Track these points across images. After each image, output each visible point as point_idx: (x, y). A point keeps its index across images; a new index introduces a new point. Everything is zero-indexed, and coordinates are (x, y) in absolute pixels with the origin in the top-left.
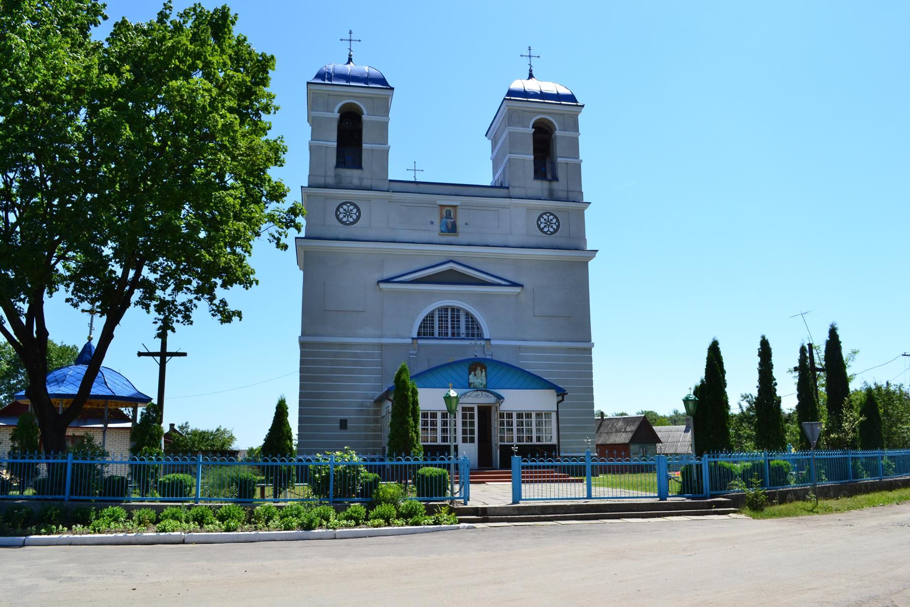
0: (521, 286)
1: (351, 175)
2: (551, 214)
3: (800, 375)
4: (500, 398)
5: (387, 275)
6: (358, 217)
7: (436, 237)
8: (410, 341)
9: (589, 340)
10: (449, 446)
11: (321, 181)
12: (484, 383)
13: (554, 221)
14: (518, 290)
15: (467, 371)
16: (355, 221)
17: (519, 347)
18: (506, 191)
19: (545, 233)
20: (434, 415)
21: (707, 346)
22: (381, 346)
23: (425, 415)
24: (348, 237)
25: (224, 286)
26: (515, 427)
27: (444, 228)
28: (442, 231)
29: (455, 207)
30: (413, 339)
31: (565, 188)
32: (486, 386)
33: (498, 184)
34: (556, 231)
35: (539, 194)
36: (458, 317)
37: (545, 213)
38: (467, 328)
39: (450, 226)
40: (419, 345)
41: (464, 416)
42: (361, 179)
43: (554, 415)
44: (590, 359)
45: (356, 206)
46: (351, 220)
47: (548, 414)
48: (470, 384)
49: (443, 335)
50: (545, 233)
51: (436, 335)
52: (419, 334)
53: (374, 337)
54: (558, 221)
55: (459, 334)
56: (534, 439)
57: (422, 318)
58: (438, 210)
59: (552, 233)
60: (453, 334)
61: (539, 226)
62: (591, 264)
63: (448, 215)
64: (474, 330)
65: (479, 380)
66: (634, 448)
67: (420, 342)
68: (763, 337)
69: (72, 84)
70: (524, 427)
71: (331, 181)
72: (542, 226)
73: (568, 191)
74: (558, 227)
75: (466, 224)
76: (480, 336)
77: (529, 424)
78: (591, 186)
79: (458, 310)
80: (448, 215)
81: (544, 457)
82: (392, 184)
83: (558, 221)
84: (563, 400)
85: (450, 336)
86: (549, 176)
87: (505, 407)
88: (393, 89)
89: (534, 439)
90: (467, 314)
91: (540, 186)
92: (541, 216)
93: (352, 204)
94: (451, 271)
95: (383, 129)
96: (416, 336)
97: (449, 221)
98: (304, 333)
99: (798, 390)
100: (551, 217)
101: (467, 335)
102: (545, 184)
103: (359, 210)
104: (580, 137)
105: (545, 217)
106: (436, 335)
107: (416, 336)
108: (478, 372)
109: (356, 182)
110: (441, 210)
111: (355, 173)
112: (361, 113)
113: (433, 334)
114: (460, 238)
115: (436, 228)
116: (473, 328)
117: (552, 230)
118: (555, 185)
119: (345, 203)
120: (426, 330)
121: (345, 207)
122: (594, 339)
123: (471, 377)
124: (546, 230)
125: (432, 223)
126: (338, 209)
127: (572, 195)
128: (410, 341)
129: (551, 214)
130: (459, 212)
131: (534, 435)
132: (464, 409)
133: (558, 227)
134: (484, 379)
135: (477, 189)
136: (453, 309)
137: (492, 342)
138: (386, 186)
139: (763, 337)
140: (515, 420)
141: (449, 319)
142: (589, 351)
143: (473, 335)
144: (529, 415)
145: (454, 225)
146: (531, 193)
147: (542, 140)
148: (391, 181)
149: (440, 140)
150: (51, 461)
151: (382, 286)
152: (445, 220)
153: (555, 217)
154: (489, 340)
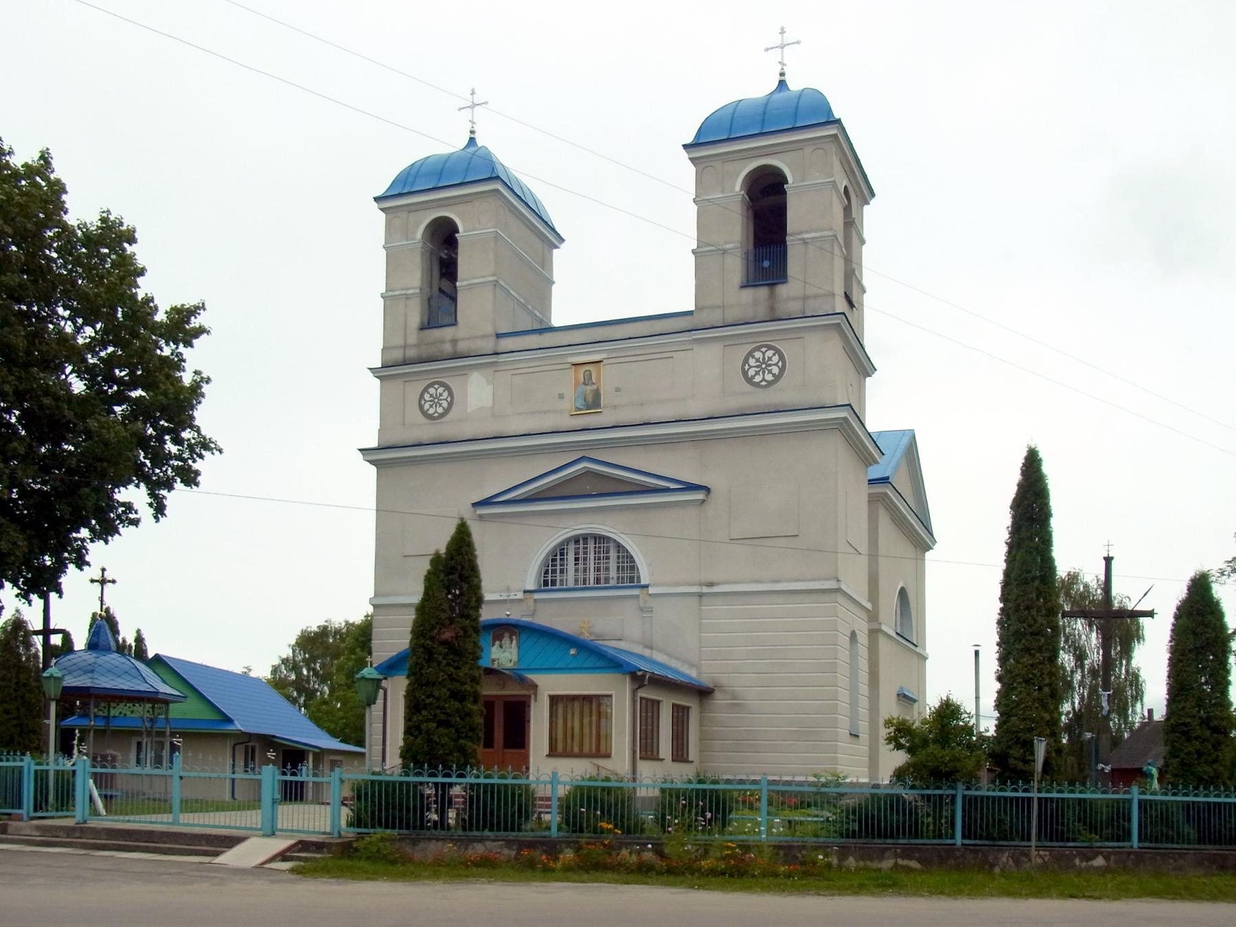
0: (707, 490)
8: (520, 596)
10: (1030, 799)
14: (700, 496)
19: (757, 385)
21: (1191, 574)
25: (97, 535)
27: (580, 403)
30: (525, 592)
31: (402, 343)
35: (749, 314)
39: (590, 399)
40: (535, 601)
50: (757, 385)
51: (571, 584)
54: (782, 358)
55: (607, 580)
60: (598, 581)
61: (745, 373)
63: (588, 380)
65: (507, 654)
72: (751, 372)
74: (782, 370)
75: (617, 390)
80: (588, 380)
83: (782, 358)
85: (613, 583)
94: (589, 473)
96: (531, 587)
97: (589, 388)
108: (506, 641)
109: (448, 348)
111: (448, 333)
112: (784, 180)
115: (568, 404)
117: (769, 377)
118: (782, 290)
125: (561, 396)
128: (520, 596)
133: (782, 370)
135: (638, 324)
137: (651, 590)
145: (597, 394)
146: (731, 315)
150: (99, 770)
152: (582, 388)
154: (646, 586)
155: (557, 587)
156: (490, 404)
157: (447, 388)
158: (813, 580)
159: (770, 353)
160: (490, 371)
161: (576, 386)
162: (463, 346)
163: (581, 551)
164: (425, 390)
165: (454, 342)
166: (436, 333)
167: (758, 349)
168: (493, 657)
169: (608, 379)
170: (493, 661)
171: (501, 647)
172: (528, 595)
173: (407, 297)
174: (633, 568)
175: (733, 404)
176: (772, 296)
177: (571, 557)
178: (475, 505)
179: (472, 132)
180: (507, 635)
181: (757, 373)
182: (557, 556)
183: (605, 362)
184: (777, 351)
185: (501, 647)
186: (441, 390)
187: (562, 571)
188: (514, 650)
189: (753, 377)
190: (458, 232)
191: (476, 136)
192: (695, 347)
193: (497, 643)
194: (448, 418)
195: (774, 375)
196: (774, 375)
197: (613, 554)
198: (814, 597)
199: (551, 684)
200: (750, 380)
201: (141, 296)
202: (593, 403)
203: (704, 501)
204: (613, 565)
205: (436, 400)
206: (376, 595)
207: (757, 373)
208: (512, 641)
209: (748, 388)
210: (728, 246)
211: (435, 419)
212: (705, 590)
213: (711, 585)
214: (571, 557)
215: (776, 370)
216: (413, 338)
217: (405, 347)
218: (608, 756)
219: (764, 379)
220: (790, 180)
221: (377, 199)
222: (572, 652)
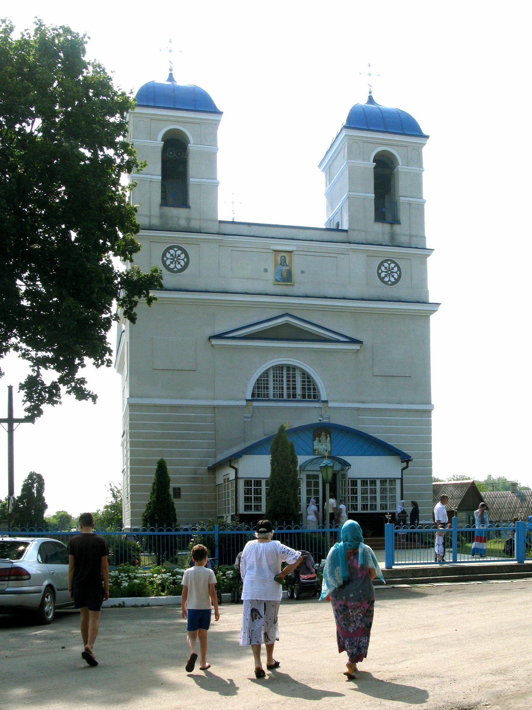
1: (178, 214)
2: (393, 262)
4: (346, 464)
5: (219, 330)
6: (187, 264)
7: (271, 288)
8: (244, 403)
9: (429, 402)
12: (329, 449)
13: (396, 269)
14: (357, 347)
15: (311, 436)
17: (358, 409)
18: (345, 234)
19: (386, 283)
20: (258, 483)
22: (214, 407)
23: (248, 483)
24: (178, 286)
26: (359, 495)
27: (278, 277)
28: (277, 281)
29: (291, 252)
30: (247, 400)
32: (330, 452)
33: (334, 226)
35: (380, 239)
36: (294, 377)
37: (386, 261)
38: (303, 389)
39: (285, 274)
40: (254, 408)
41: (308, 484)
42: (188, 219)
43: (398, 482)
44: (429, 423)
45: (184, 251)
46: (179, 267)
47: (392, 481)
48: (314, 451)
49: (280, 397)
50: (386, 283)
51: (271, 397)
52: (253, 395)
53: (206, 399)
54: (399, 269)
55: (294, 396)
56: (378, 507)
57: (257, 377)
58: (272, 256)
59: (393, 283)
60: (289, 396)
61: (379, 275)
62: (432, 317)
63: (283, 262)
64: (310, 392)
65: (324, 446)
67: (255, 404)
68: (95, 403)
69: (50, 177)
70: (253, 496)
71: (156, 221)
72: (383, 275)
73: (411, 236)
75: (303, 272)
76: (316, 397)
77: (374, 491)
78: (434, 232)
79: (294, 368)
80: (283, 262)
81: (400, 525)
82: (223, 225)
83: (399, 269)
84: (407, 467)
85: (299, 398)
86: (389, 217)
87: (352, 473)
88: (221, 113)
89: (378, 507)
90: (304, 374)
91: (381, 230)
92: (382, 264)
93: (180, 248)
94: (287, 325)
95: (211, 159)
96: (249, 397)
97: (285, 268)
100: (392, 265)
101: (304, 396)
102: (387, 227)
103: (187, 256)
104: (424, 174)
106: (271, 397)
107: (249, 397)
108: (323, 437)
109: (183, 223)
110: (276, 256)
111: (181, 212)
114: (296, 289)
115: (270, 276)
116: (309, 389)
117: (392, 280)
118: (397, 228)
119: (172, 248)
120: (259, 392)
121: (172, 252)
122: (434, 400)
123: (315, 443)
124: (386, 279)
125: (266, 270)
126: (164, 255)
127: (415, 242)
129: (393, 262)
130: (296, 259)
131: (378, 502)
132: (308, 477)
134: (329, 445)
135: (306, 231)
136: (289, 368)
137: (330, 404)
138: (215, 228)
139: (95, 403)
140: (359, 487)
141: (285, 379)
142: (428, 412)
143: (309, 396)
144: (373, 482)
145: (290, 273)
146: (371, 238)
148: (221, 222)
149: (272, 176)
151: (214, 342)
152: (280, 267)
153: (397, 265)
154: (326, 402)
155: (312, 399)
162: (195, 224)
171: (320, 441)
176: (392, 229)
177: (271, 378)
179: (171, 70)
180: (323, 434)
181: (386, 276)
183: (295, 253)
186: (182, 263)
189: (395, 279)
191: (173, 72)
192: (350, 253)
193: (317, 438)
200: (382, 279)
201: (375, 164)
202: (287, 278)
203: (358, 350)
207: (386, 276)
209: (380, 283)
214: (271, 378)
215: (396, 276)
217: (150, 216)
219: (389, 280)
220: (400, 163)
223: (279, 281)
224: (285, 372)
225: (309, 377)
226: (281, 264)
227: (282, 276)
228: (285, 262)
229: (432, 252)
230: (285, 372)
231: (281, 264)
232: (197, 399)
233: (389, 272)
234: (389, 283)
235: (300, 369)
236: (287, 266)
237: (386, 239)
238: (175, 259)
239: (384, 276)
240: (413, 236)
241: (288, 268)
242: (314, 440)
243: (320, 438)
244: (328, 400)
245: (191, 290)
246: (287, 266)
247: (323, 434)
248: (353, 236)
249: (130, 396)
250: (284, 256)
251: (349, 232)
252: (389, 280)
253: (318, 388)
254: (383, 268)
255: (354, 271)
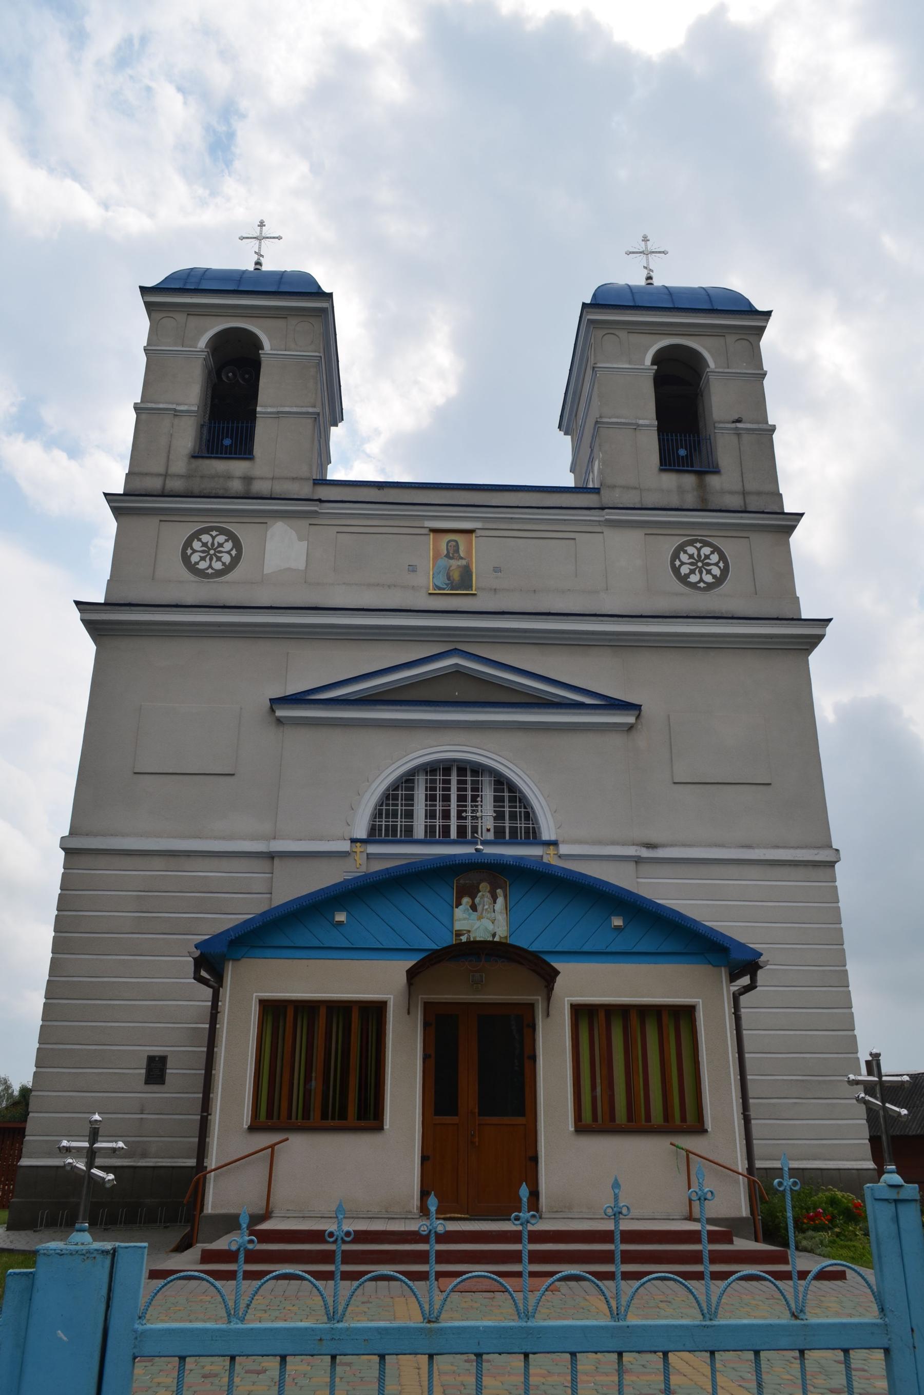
0: (636, 708)
3: (657, 371)
5: (291, 690)
11: (154, 484)
13: (715, 558)
16: (228, 569)
19: (694, 586)
27: (441, 580)
30: (354, 841)
31: (738, 487)
34: (719, 581)
39: (456, 576)
50: (694, 586)
51: (419, 832)
53: (254, 838)
54: (722, 557)
59: (710, 587)
60: (462, 831)
61: (676, 571)
63: (453, 552)
66: (477, 900)
67: (373, 849)
72: (684, 570)
73: (744, 494)
74: (725, 571)
75: (497, 570)
79: (478, 770)
80: (453, 552)
83: (722, 557)
88: (330, 296)
94: (458, 673)
96: (362, 834)
97: (454, 563)
98: (74, 831)
99: (658, 418)
101: (499, 832)
102: (689, 480)
105: (691, 550)
106: (419, 832)
107: (362, 834)
108: (483, 898)
109: (236, 486)
111: (238, 467)
113: (409, 830)
117: (708, 579)
118: (713, 481)
123: (459, 912)
124: (694, 578)
125: (413, 569)
128: (345, 846)
137: (564, 849)
145: (466, 572)
147: (678, 386)
152: (443, 562)
154: (555, 843)
156: (302, 566)
157: (232, 537)
158: (777, 847)
159: (706, 550)
160: (304, 523)
161: (435, 558)
162: (260, 487)
163: (439, 785)
164: (196, 535)
165: (248, 480)
166: (219, 466)
167: (691, 543)
168: (458, 926)
169: (482, 555)
170: (459, 934)
171: (474, 908)
172: (359, 847)
173: (176, 414)
174: (529, 815)
175: (662, 605)
176: (702, 487)
177: (420, 795)
178: (276, 702)
180: (484, 887)
182: (398, 794)
183: (479, 533)
184: (716, 549)
185: (474, 908)
187: (474, 799)
188: (501, 918)
190: (262, 349)
193: (466, 900)
194: (229, 577)
195: (687, 576)
196: (687, 576)
197: (488, 793)
198: (801, 872)
199: (585, 982)
200: (684, 579)
201: (656, 367)
202: (463, 582)
204: (487, 809)
205: (211, 552)
206: (73, 832)
207: (692, 572)
208: (494, 899)
209: (687, 590)
210: (641, 422)
211: (208, 576)
212: (645, 853)
213: (650, 846)
214: (420, 795)
215: (716, 571)
216: (180, 466)
217: (166, 475)
218: (699, 1129)
219: (701, 580)
220: (712, 364)
221: (144, 290)
222: (618, 922)
223: (440, 589)
224: (454, 778)
225: (513, 788)
226: (447, 556)
227: (449, 579)
228: (457, 550)
229: (798, 521)
230: (454, 778)
231: (447, 556)
232: (231, 838)
233: (700, 564)
234: (702, 585)
235: (492, 771)
236: (462, 558)
237: (690, 500)
238: (212, 552)
239: (687, 571)
240: (750, 493)
241: (464, 562)
242: (459, 904)
243: (473, 898)
244: (560, 839)
245: (233, 604)
246: (462, 558)
247: (484, 887)
248: (608, 497)
249: (71, 833)
250: (456, 541)
251: (602, 492)
252: (701, 580)
253: (534, 812)
254: (684, 557)
255: (622, 570)
